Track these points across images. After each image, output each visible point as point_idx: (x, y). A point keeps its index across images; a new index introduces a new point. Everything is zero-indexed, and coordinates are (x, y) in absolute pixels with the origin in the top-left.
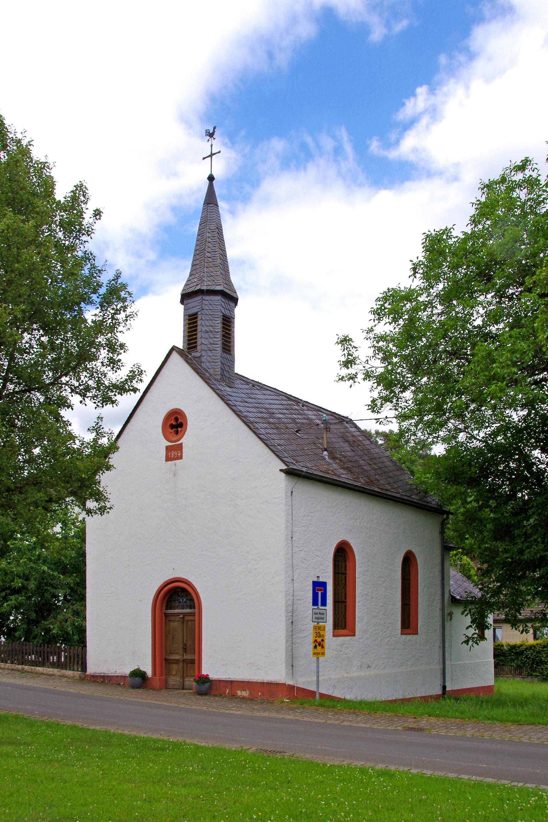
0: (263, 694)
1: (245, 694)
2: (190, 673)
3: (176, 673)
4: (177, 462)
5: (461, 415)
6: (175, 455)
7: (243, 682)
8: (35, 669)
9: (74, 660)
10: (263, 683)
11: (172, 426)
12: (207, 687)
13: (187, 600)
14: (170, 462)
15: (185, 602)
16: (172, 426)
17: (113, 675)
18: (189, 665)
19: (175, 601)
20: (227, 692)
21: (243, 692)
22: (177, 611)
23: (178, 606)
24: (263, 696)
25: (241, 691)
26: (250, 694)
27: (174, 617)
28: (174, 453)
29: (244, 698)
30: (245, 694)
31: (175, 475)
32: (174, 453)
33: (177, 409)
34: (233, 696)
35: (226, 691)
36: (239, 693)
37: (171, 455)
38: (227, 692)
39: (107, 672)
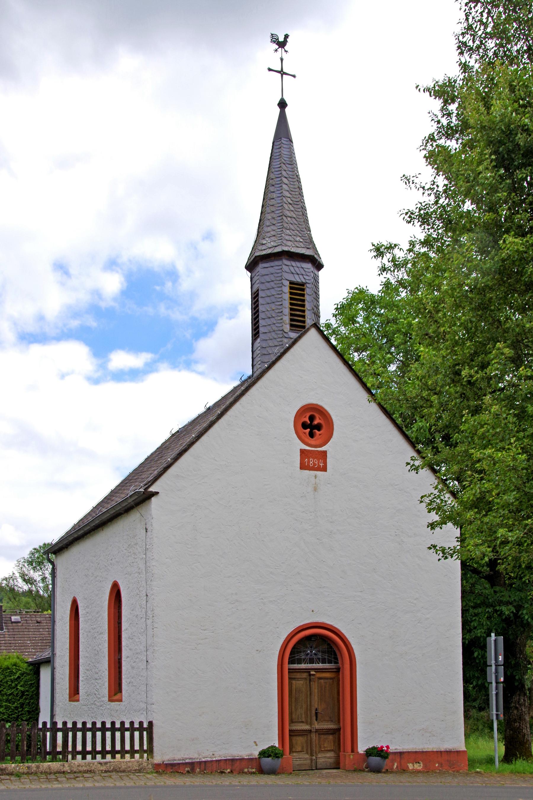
0: (441, 765)
1: (418, 767)
2: (324, 747)
3: (303, 748)
4: (319, 473)
5: (398, 347)
6: (315, 464)
7: (416, 752)
8: (38, 767)
9: (497, 694)
10: (441, 752)
11: (305, 426)
12: (379, 759)
13: (319, 651)
14: (307, 472)
15: (315, 654)
16: (305, 426)
17: (209, 759)
18: (322, 736)
19: (301, 652)
20: (395, 766)
21: (415, 765)
22: (303, 666)
23: (304, 659)
24: (442, 767)
25: (413, 763)
26: (425, 766)
27: (299, 674)
28: (313, 461)
29: (419, 772)
30: (418, 767)
31: (315, 489)
32: (313, 461)
33: (317, 405)
34: (403, 770)
35: (393, 765)
36: (410, 766)
37: (309, 462)
38: (395, 766)
39: (196, 756)
